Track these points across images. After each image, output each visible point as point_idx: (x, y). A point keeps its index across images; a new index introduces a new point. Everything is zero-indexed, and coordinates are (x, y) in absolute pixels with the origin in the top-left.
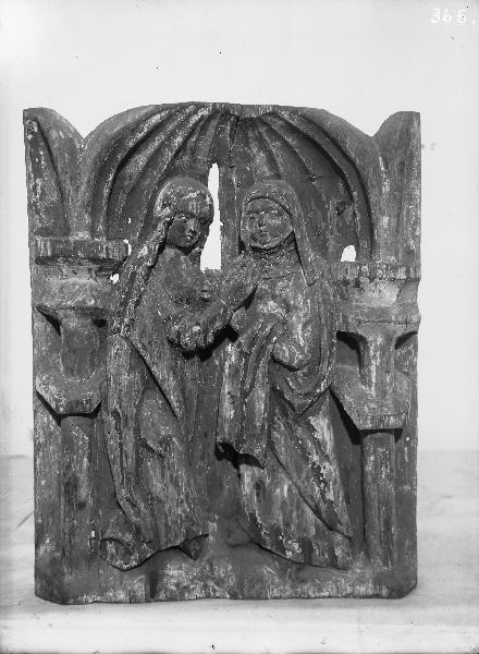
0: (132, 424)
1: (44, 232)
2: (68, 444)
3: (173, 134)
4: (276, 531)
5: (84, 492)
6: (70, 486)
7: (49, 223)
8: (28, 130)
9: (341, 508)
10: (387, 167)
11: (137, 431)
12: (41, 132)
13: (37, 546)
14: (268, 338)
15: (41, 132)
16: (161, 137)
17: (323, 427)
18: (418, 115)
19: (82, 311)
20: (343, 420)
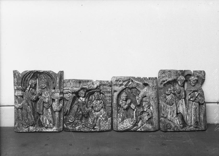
0: (26, 110)
1: (18, 89)
2: (18, 112)
3: (31, 74)
4: (44, 123)
5: (20, 118)
6: (18, 118)
7: (16, 84)
8: (13, 73)
9: (52, 120)
10: (136, 117)
11: (27, 111)
12: (15, 73)
13: (15, 125)
14: (43, 99)
15: (15, 73)
16: (30, 74)
17: (49, 110)
18: (63, 72)
19: (20, 96)
20: (52, 109)
